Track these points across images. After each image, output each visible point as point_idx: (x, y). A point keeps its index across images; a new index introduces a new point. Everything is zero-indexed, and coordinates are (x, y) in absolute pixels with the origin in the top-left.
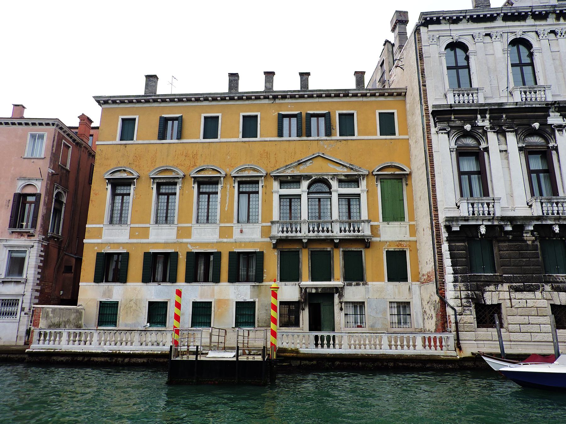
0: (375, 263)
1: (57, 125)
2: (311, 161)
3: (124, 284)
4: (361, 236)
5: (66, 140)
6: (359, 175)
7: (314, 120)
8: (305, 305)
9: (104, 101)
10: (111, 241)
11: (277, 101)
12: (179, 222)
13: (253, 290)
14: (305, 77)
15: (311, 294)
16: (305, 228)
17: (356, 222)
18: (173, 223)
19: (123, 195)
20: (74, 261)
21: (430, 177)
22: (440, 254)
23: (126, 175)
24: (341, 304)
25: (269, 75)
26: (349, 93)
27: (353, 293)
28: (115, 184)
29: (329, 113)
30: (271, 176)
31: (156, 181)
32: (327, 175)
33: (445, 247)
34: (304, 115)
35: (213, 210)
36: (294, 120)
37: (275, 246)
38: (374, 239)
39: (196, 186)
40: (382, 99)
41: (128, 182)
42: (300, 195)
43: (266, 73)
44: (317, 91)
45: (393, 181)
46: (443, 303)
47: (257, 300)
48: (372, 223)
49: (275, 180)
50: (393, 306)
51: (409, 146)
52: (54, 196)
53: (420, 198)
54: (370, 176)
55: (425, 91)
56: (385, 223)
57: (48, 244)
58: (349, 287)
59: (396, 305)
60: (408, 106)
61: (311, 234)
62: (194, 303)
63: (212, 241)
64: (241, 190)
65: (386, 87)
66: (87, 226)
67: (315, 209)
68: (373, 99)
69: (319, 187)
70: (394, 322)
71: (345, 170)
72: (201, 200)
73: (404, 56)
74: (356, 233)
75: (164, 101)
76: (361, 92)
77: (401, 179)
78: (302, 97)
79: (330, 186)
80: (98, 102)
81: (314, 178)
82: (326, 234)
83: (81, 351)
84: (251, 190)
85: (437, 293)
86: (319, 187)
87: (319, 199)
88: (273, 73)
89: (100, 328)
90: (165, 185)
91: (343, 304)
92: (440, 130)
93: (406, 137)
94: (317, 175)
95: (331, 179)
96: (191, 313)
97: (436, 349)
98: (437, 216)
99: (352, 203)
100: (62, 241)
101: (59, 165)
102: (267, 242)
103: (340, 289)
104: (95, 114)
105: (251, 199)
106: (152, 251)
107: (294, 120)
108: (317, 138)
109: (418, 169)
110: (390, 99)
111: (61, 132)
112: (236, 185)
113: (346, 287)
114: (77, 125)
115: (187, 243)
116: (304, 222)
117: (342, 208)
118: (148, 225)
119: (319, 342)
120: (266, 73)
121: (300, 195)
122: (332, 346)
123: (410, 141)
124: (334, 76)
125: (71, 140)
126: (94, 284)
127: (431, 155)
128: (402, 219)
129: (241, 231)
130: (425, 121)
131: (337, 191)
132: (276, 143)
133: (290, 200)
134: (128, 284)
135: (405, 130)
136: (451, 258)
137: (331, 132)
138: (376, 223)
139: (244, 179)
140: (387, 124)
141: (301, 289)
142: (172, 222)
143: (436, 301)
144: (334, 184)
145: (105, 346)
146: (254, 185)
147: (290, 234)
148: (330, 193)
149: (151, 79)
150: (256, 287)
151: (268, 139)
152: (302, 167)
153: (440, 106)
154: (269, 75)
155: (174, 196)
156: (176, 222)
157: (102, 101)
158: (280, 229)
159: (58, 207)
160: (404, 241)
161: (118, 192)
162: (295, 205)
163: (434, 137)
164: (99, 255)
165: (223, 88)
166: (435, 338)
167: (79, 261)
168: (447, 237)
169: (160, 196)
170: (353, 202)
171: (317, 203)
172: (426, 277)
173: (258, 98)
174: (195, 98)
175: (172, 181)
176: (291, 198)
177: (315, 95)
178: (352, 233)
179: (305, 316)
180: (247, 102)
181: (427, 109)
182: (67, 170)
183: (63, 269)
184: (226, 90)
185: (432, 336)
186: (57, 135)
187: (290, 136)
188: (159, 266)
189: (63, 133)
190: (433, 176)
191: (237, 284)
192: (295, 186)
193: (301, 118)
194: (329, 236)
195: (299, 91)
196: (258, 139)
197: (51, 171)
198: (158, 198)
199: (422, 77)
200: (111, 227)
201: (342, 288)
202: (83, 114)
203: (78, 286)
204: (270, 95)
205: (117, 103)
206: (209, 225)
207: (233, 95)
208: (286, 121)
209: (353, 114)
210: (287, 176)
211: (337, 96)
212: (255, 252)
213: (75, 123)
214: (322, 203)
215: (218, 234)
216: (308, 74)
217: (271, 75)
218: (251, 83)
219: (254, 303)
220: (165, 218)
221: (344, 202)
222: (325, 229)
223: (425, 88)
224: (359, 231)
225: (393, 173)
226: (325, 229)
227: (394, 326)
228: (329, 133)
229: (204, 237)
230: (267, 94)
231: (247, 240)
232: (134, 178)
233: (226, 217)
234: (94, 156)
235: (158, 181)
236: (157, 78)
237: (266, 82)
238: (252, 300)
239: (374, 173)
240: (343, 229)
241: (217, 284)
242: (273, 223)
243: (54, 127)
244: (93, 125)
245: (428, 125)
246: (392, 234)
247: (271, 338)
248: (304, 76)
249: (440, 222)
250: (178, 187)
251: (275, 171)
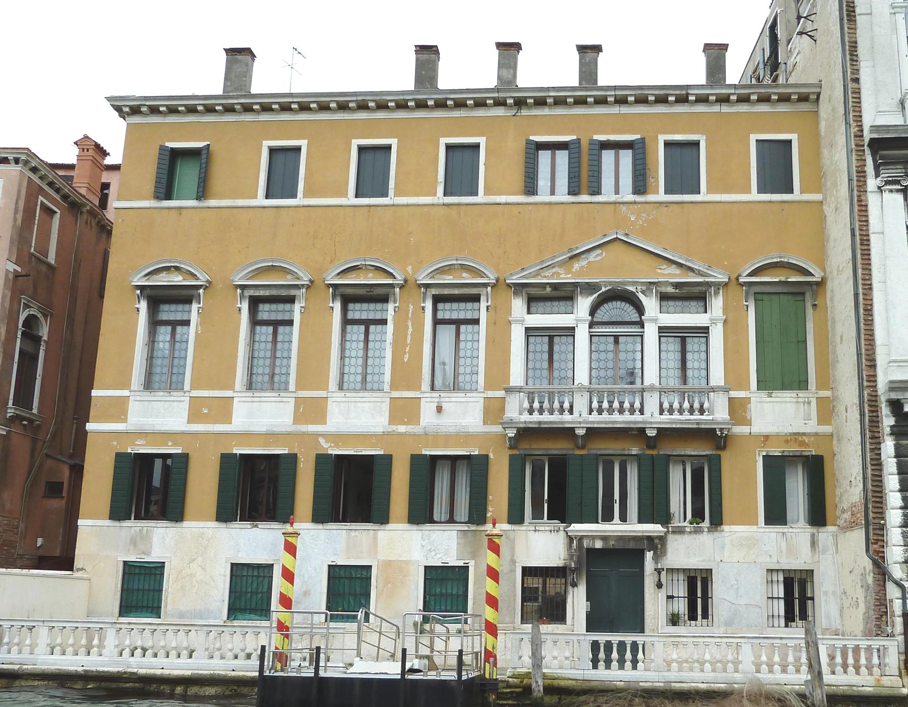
0: (744, 480)
1: (26, 163)
2: (599, 251)
3: (178, 525)
4: (707, 422)
5: (46, 195)
6: (708, 285)
7: (608, 156)
8: (579, 576)
9: (131, 107)
10: (148, 428)
11: (524, 112)
12: (300, 386)
13: (462, 541)
14: (590, 55)
15: (591, 551)
16: (581, 403)
17: (701, 392)
18: (286, 389)
19: (174, 324)
20: (66, 472)
21: (861, 291)
22: (878, 464)
23: (181, 278)
24: (659, 573)
25: (509, 50)
26: (688, 94)
27: (687, 550)
28: (158, 298)
29: (643, 140)
30: (509, 285)
31: (248, 293)
32: (634, 283)
33: (888, 446)
34: (585, 145)
35: (469, 345)
36: (562, 157)
37: (514, 443)
38: (738, 430)
39: (337, 306)
40: (763, 108)
41: (184, 296)
42: (573, 329)
43: (500, 46)
44: (615, 88)
45: (784, 298)
46: (881, 572)
47: (472, 565)
48: (734, 394)
49: (516, 294)
50: (775, 579)
51: (823, 218)
52: (20, 326)
53: (841, 337)
54: (733, 287)
55: (857, 92)
56: (763, 394)
57: (8, 432)
58: (677, 537)
59: (781, 578)
60: (823, 124)
61: (595, 417)
62: (333, 570)
63: (372, 430)
64: (440, 315)
65: (781, 80)
66: (94, 393)
67: (541, 369)
68: (743, 108)
69: (613, 312)
70: (776, 614)
71: (673, 270)
72: (348, 337)
73: (818, 9)
74: (696, 417)
75: (266, 108)
76: (714, 93)
77: (803, 294)
78: (581, 102)
79: (640, 309)
80: (118, 109)
81: (604, 289)
82: (627, 417)
83: (80, 669)
84: (462, 316)
85: (867, 550)
86: (613, 312)
87: (616, 338)
88: (517, 47)
89: (122, 620)
90: (268, 305)
91: (664, 573)
92: (887, 183)
93: (818, 197)
94: (610, 283)
95: (643, 292)
96: (325, 591)
97: (858, 673)
98: (873, 378)
99: (689, 347)
100: (39, 426)
101: (32, 255)
102: (497, 435)
103: (656, 541)
104: (113, 135)
105: (462, 337)
106: (238, 451)
107: (562, 157)
108: (613, 198)
109: (839, 272)
110: (783, 108)
111: (35, 178)
112: (429, 305)
113: (670, 537)
114: (73, 160)
115: (317, 435)
116: (581, 388)
117: (667, 360)
118: (228, 393)
119: (602, 655)
120: (500, 46)
121: (573, 329)
122: (628, 664)
123: (825, 207)
124: (654, 55)
125: (57, 197)
126: (108, 522)
127: (865, 241)
128: (802, 385)
129: (439, 409)
130: (854, 163)
131: (655, 320)
132: (521, 208)
133: (551, 338)
134: (185, 524)
135: (816, 181)
136: (899, 474)
137: (645, 186)
138: (741, 394)
139: (446, 291)
140: (776, 168)
141: (571, 539)
142: (283, 386)
143: (865, 568)
144: (650, 304)
145: (132, 659)
146: (469, 305)
147: (546, 417)
148: (641, 324)
149: (239, 58)
150: (469, 534)
151: (502, 199)
152: (576, 266)
153: (887, 128)
154: (509, 50)
155: (288, 328)
156: (292, 387)
157: (128, 108)
158: (526, 405)
159: (29, 348)
160: (804, 434)
161: (164, 316)
162: (560, 352)
163: (873, 200)
164: (121, 458)
165: (402, 79)
166: (856, 650)
167: (78, 471)
168: (892, 427)
169: (258, 328)
170: (693, 344)
171: (611, 347)
172: (847, 516)
173: (480, 104)
174: (337, 102)
175: (284, 293)
176: (552, 334)
177: (612, 99)
178: (686, 416)
179: (578, 602)
180: (457, 113)
181: (860, 135)
182: (49, 265)
183: (42, 489)
184: (411, 86)
185: (851, 644)
186: (25, 183)
187: (553, 193)
188: (255, 487)
189: (38, 181)
190: (869, 288)
191: (428, 527)
192: (563, 309)
193: (579, 153)
194: (636, 422)
195: (573, 89)
196: (481, 198)
197: (12, 267)
198: (253, 332)
199: (852, 60)
200: (147, 396)
201: (663, 539)
202: (86, 137)
203: (76, 527)
204: (510, 99)
205: (160, 112)
206: (366, 394)
207: (427, 96)
208: (544, 157)
209: (696, 144)
210: (543, 286)
211: (662, 100)
212: (468, 457)
213: (70, 156)
214: (622, 347)
215: (387, 414)
216: (724, 47)
217: (512, 52)
218: (467, 69)
219: (466, 568)
220: (265, 379)
221: (673, 345)
222: (627, 405)
223: (855, 85)
224: (702, 411)
225: (783, 279)
226: (627, 405)
227: (776, 624)
228: (641, 185)
229: (356, 420)
230: (502, 95)
231: (452, 430)
232: (200, 287)
233: (405, 376)
234: (109, 233)
235: (252, 292)
236: (253, 56)
237: (501, 66)
238: (461, 563)
239: (741, 280)
240: (666, 405)
241: (383, 527)
242: (509, 390)
243: (18, 168)
244: (108, 161)
245: (862, 174)
246: (778, 416)
247: (277, 638)
248: (589, 53)
249: (879, 393)
250: (297, 307)
251: (517, 273)
